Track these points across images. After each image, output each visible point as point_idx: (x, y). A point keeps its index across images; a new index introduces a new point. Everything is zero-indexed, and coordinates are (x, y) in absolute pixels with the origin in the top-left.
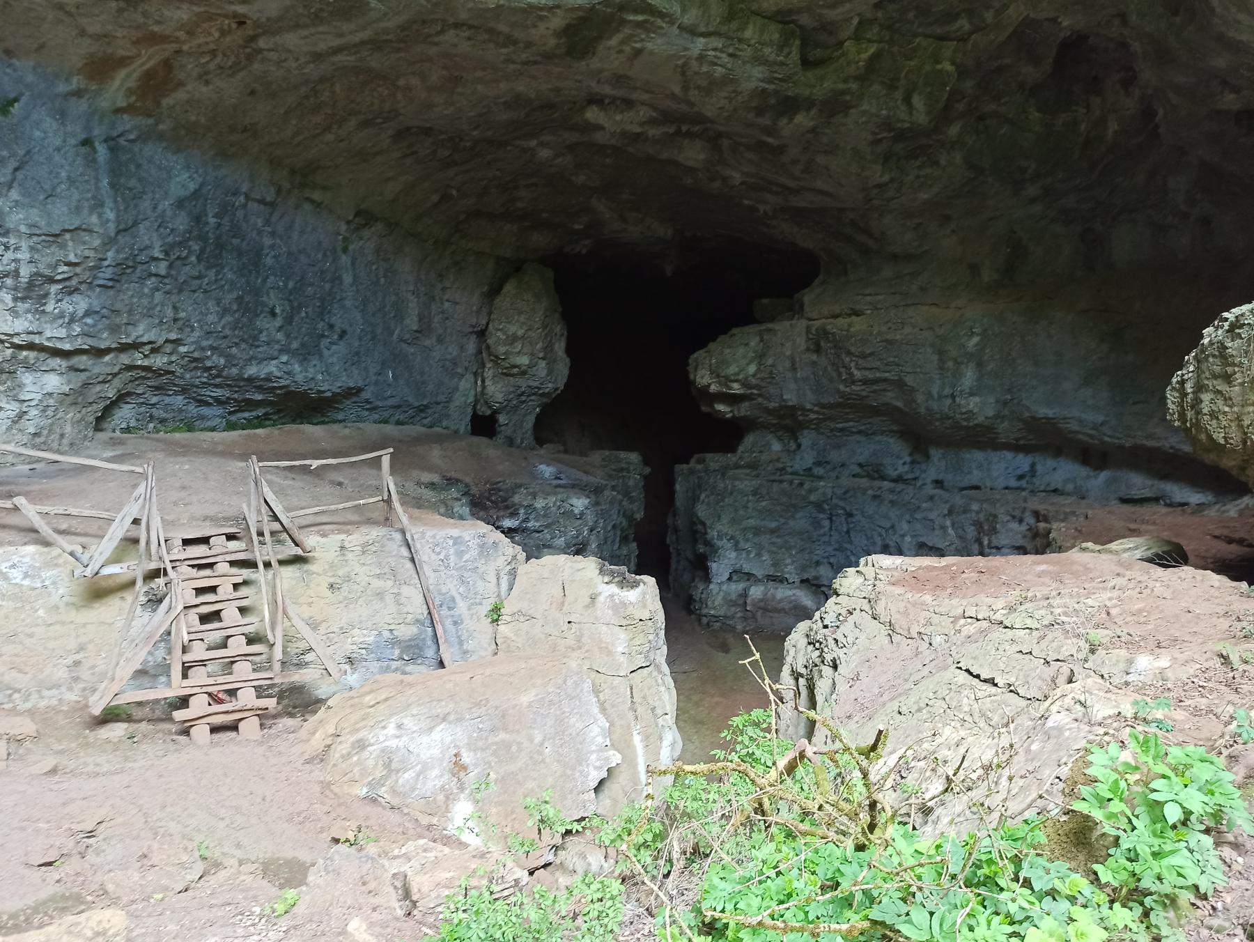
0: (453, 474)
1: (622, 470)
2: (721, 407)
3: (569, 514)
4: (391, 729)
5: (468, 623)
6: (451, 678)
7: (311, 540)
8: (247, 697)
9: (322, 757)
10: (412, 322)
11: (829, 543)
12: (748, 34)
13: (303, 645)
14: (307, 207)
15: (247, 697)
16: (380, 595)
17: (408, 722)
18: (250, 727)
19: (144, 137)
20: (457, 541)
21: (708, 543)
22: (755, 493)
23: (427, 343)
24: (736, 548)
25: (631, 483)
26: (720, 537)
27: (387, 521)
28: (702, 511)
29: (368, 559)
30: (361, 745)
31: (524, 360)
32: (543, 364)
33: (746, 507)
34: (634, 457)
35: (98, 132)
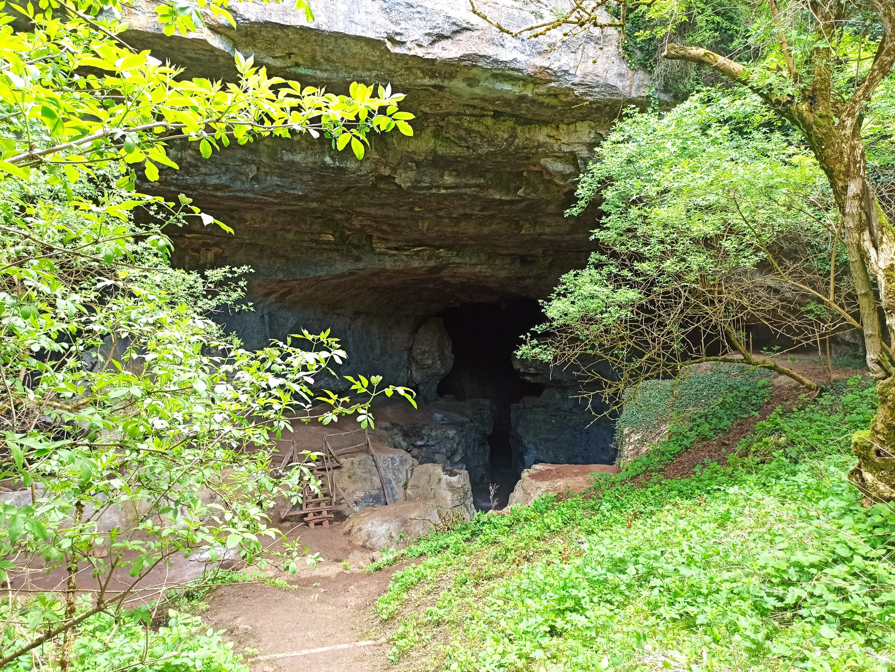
0: (395, 421)
1: (480, 409)
2: (528, 378)
3: (447, 438)
4: (370, 525)
5: (396, 489)
6: (390, 508)
7: (342, 460)
8: (325, 513)
9: (348, 533)
10: (378, 351)
11: (581, 446)
12: (497, 262)
13: (341, 497)
14: (335, 316)
15: (325, 513)
16: (365, 479)
17: (375, 522)
18: (326, 524)
19: (279, 309)
20: (392, 459)
21: (524, 446)
22: (544, 421)
23: (385, 359)
24: (536, 449)
25: (485, 416)
26: (529, 443)
27: (367, 452)
28: (520, 430)
29: (361, 466)
30: (360, 529)
31: (430, 362)
32: (439, 362)
33: (540, 428)
34: (487, 402)
35: (265, 312)
